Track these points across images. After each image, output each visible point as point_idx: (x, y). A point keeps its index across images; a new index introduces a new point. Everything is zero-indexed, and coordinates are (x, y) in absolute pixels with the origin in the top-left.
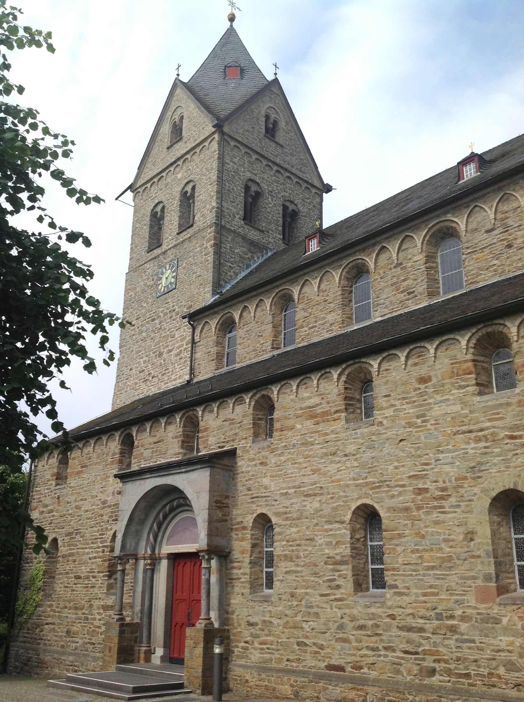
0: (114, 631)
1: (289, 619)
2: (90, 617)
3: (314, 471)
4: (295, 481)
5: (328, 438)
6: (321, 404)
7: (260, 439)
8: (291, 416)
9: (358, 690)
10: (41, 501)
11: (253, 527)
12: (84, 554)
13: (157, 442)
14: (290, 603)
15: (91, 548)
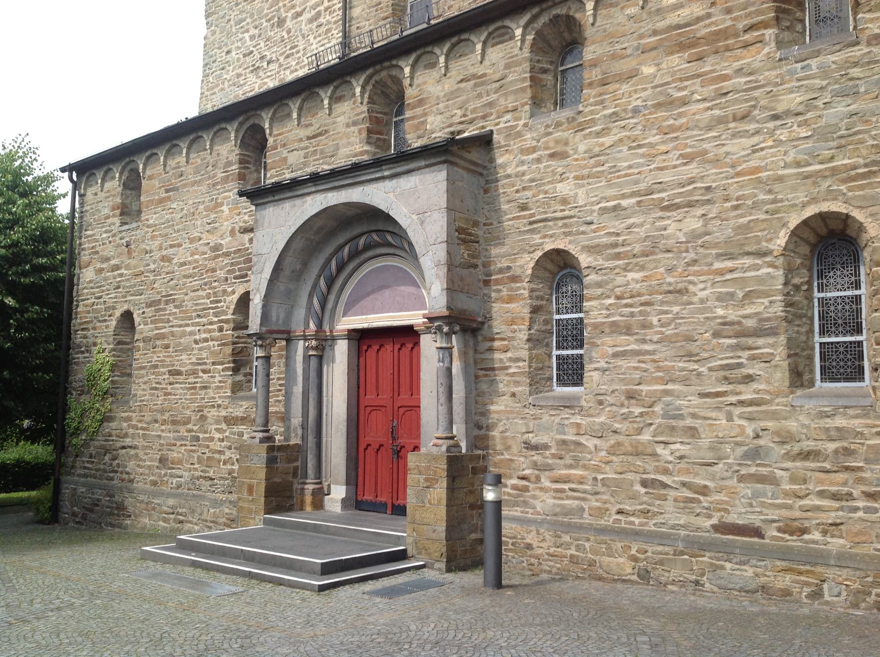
0: (256, 459)
1: (621, 438)
2: (201, 435)
3: (688, 159)
4: (636, 182)
5: (727, 85)
6: (709, 15)
7: (543, 110)
8: (629, 52)
9: (800, 573)
10: (97, 252)
11: (534, 277)
12: (184, 334)
13: (314, 137)
14: (625, 410)
15: (198, 324)
